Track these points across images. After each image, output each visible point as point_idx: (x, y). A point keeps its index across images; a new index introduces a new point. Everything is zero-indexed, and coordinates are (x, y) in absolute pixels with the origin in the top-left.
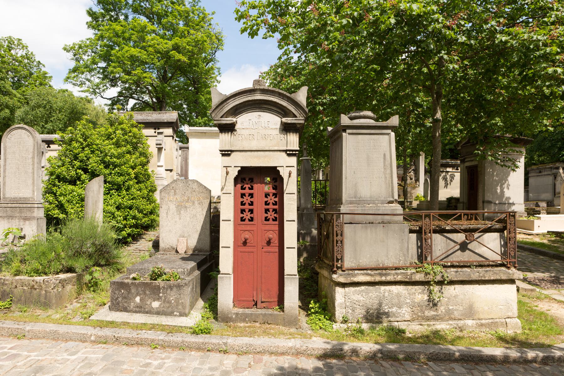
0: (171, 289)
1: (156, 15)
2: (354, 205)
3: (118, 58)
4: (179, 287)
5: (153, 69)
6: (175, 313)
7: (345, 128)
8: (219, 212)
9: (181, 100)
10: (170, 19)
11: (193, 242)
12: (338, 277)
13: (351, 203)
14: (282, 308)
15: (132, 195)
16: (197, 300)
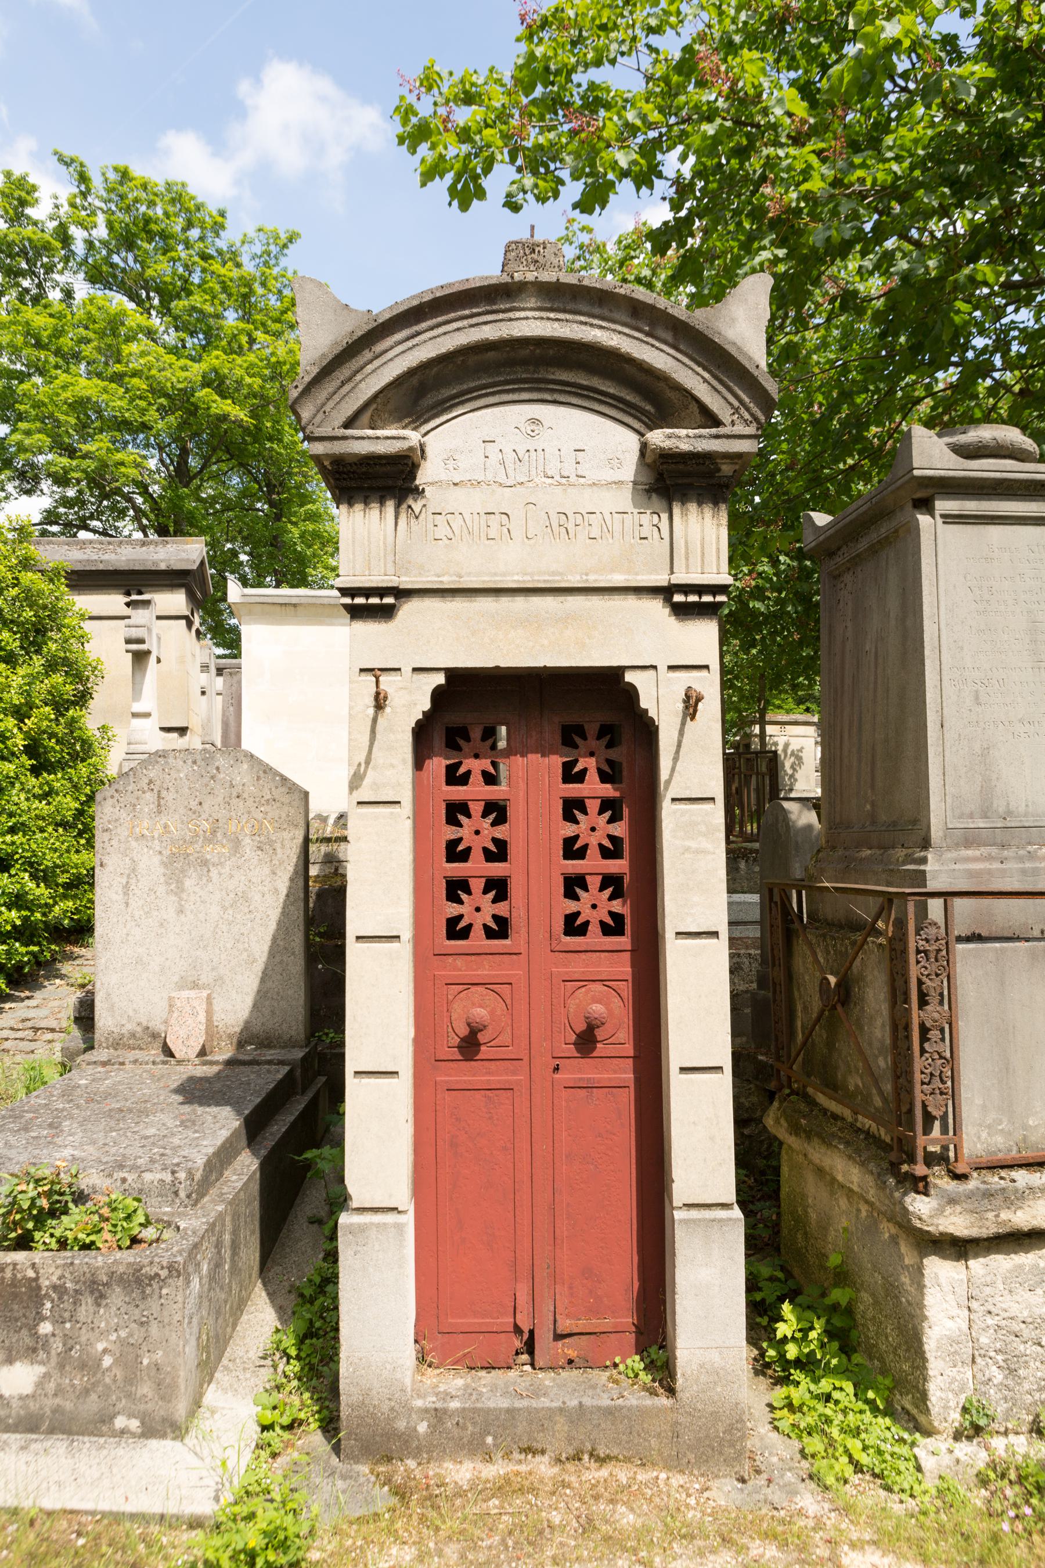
0: (100, 1298)
1: (158, 291)
2: (984, 850)
3: (38, 405)
4: (138, 1283)
5: (147, 446)
6: (120, 1422)
7: (927, 493)
8: (344, 876)
9: (232, 540)
10: (197, 299)
11: (236, 1006)
12: (940, 1211)
13: (970, 839)
14: (663, 1372)
15: (11, 815)
16: (240, 1307)
